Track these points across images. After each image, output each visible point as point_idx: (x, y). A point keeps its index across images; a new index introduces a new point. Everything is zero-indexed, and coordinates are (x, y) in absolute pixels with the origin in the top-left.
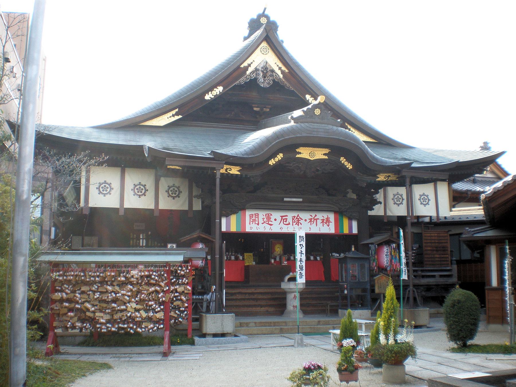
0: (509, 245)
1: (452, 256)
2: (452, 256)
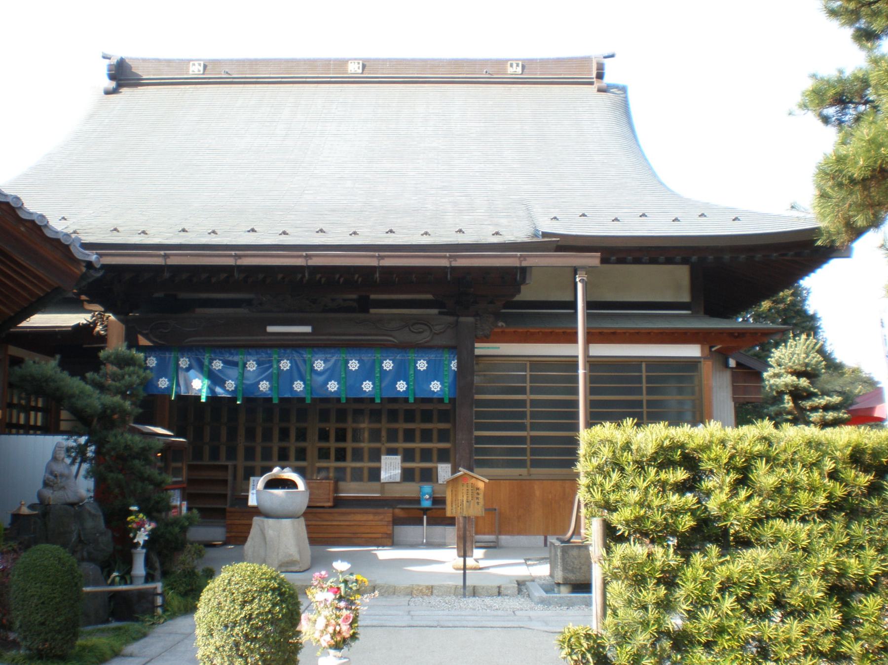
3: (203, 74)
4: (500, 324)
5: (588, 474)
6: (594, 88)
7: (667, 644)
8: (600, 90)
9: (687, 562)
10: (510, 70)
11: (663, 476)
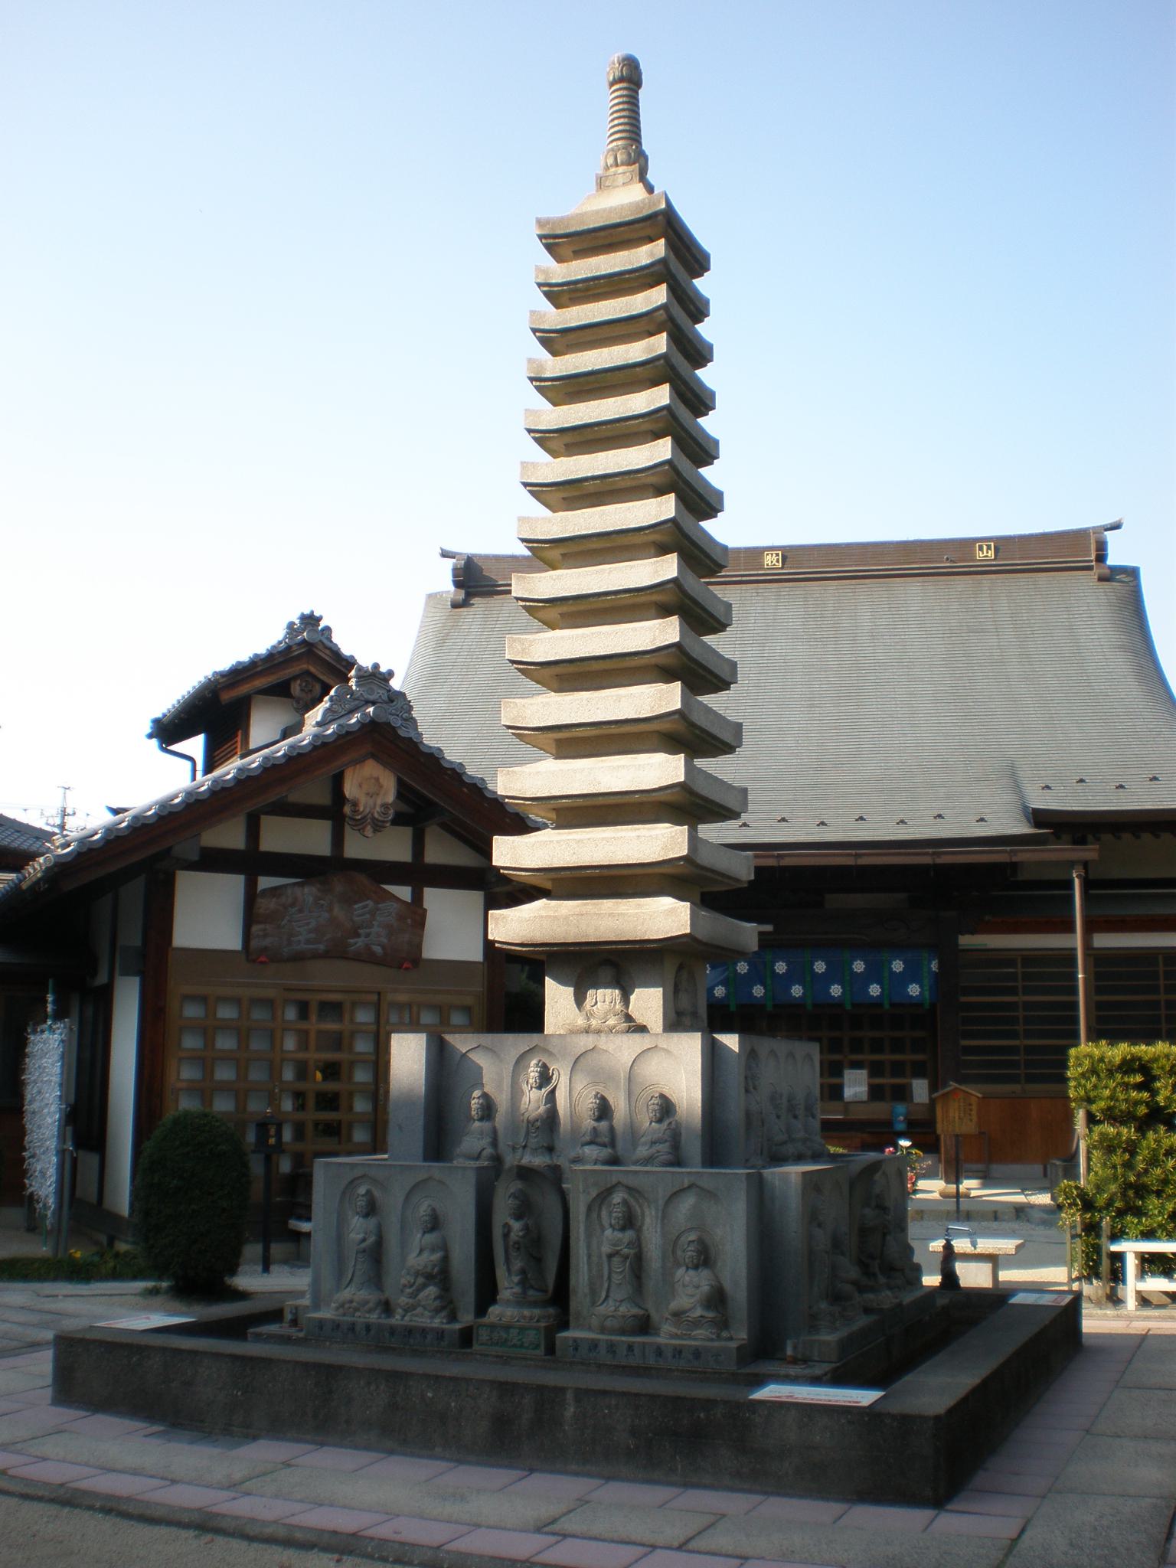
4: (987, 918)
5: (1075, 1079)
6: (1093, 575)
7: (1131, 1193)
8: (1101, 579)
9: (1144, 1136)
10: (979, 555)
11: (1126, 1079)
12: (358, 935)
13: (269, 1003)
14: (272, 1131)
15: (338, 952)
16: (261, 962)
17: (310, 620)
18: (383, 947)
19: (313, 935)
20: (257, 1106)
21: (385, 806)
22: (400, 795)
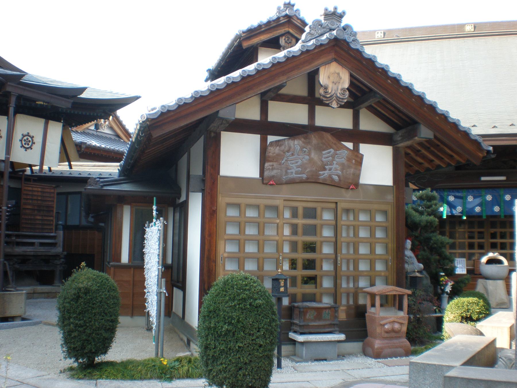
0: (156, 206)
1: (58, 219)
2: (58, 219)
3: (384, 38)
12: (325, 169)
13: (275, 208)
14: (282, 283)
15: (313, 180)
16: (271, 185)
17: (289, 5)
18: (339, 176)
19: (300, 169)
20: (269, 267)
21: (343, 89)
22: (352, 84)
